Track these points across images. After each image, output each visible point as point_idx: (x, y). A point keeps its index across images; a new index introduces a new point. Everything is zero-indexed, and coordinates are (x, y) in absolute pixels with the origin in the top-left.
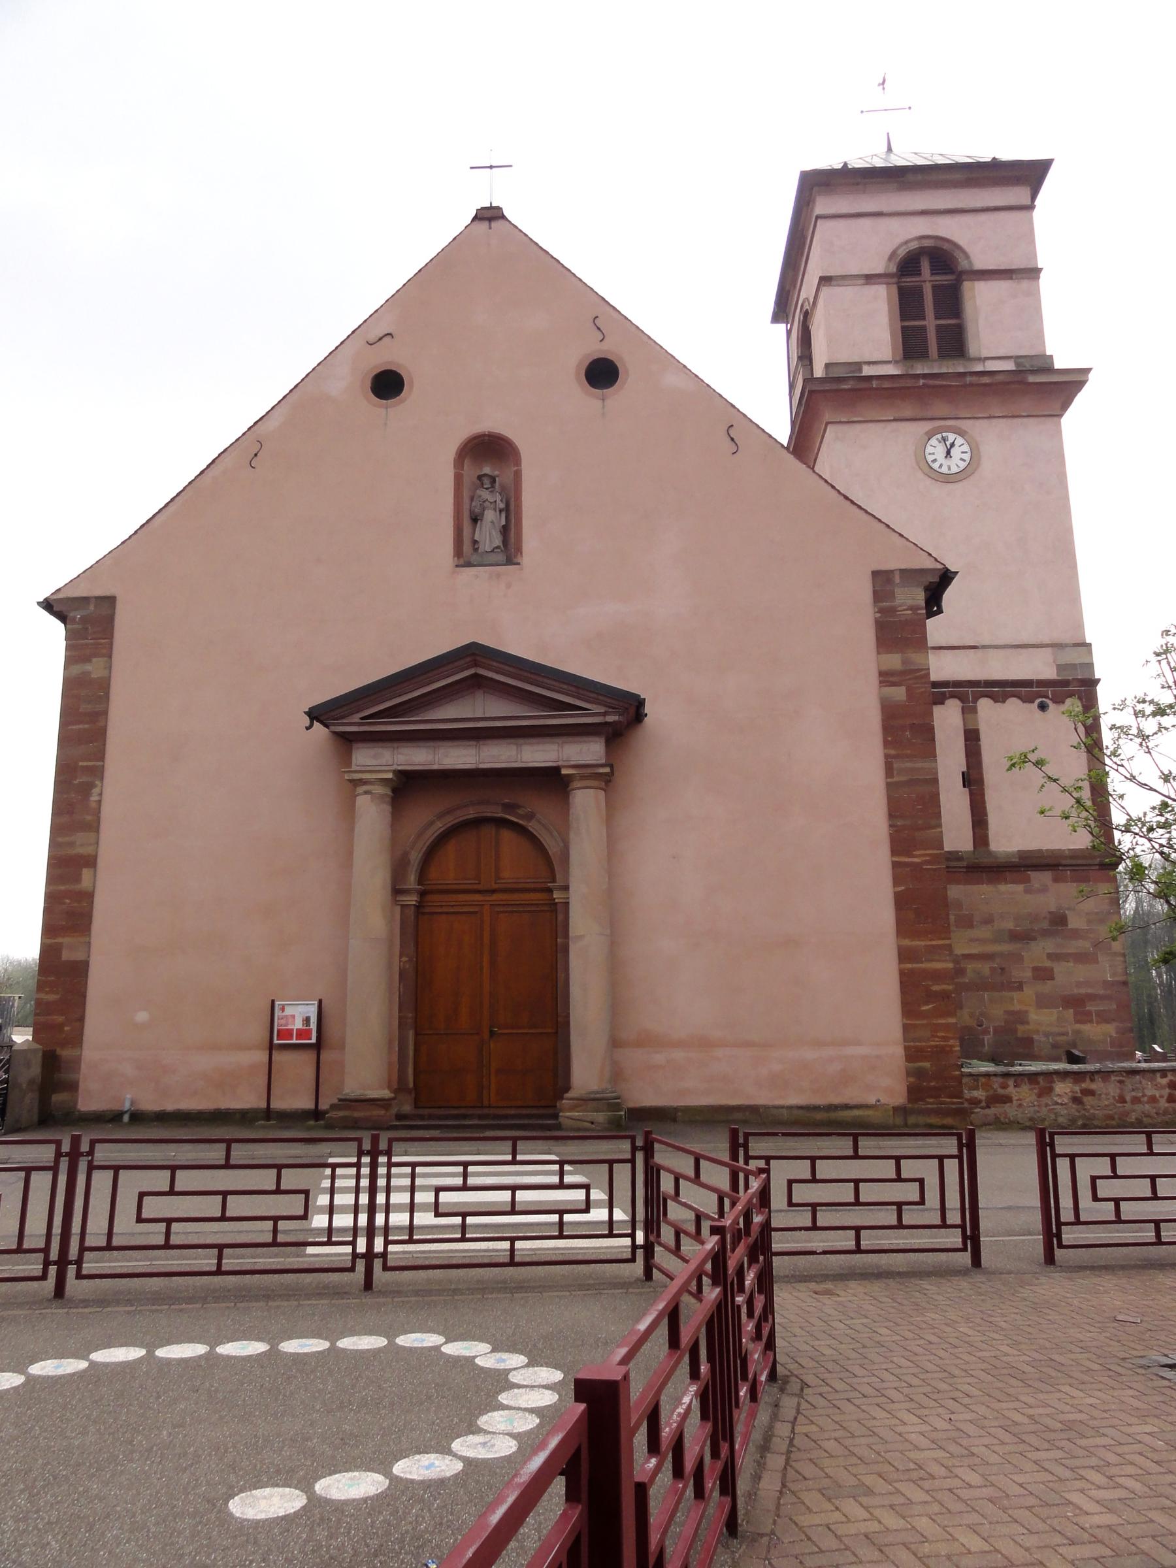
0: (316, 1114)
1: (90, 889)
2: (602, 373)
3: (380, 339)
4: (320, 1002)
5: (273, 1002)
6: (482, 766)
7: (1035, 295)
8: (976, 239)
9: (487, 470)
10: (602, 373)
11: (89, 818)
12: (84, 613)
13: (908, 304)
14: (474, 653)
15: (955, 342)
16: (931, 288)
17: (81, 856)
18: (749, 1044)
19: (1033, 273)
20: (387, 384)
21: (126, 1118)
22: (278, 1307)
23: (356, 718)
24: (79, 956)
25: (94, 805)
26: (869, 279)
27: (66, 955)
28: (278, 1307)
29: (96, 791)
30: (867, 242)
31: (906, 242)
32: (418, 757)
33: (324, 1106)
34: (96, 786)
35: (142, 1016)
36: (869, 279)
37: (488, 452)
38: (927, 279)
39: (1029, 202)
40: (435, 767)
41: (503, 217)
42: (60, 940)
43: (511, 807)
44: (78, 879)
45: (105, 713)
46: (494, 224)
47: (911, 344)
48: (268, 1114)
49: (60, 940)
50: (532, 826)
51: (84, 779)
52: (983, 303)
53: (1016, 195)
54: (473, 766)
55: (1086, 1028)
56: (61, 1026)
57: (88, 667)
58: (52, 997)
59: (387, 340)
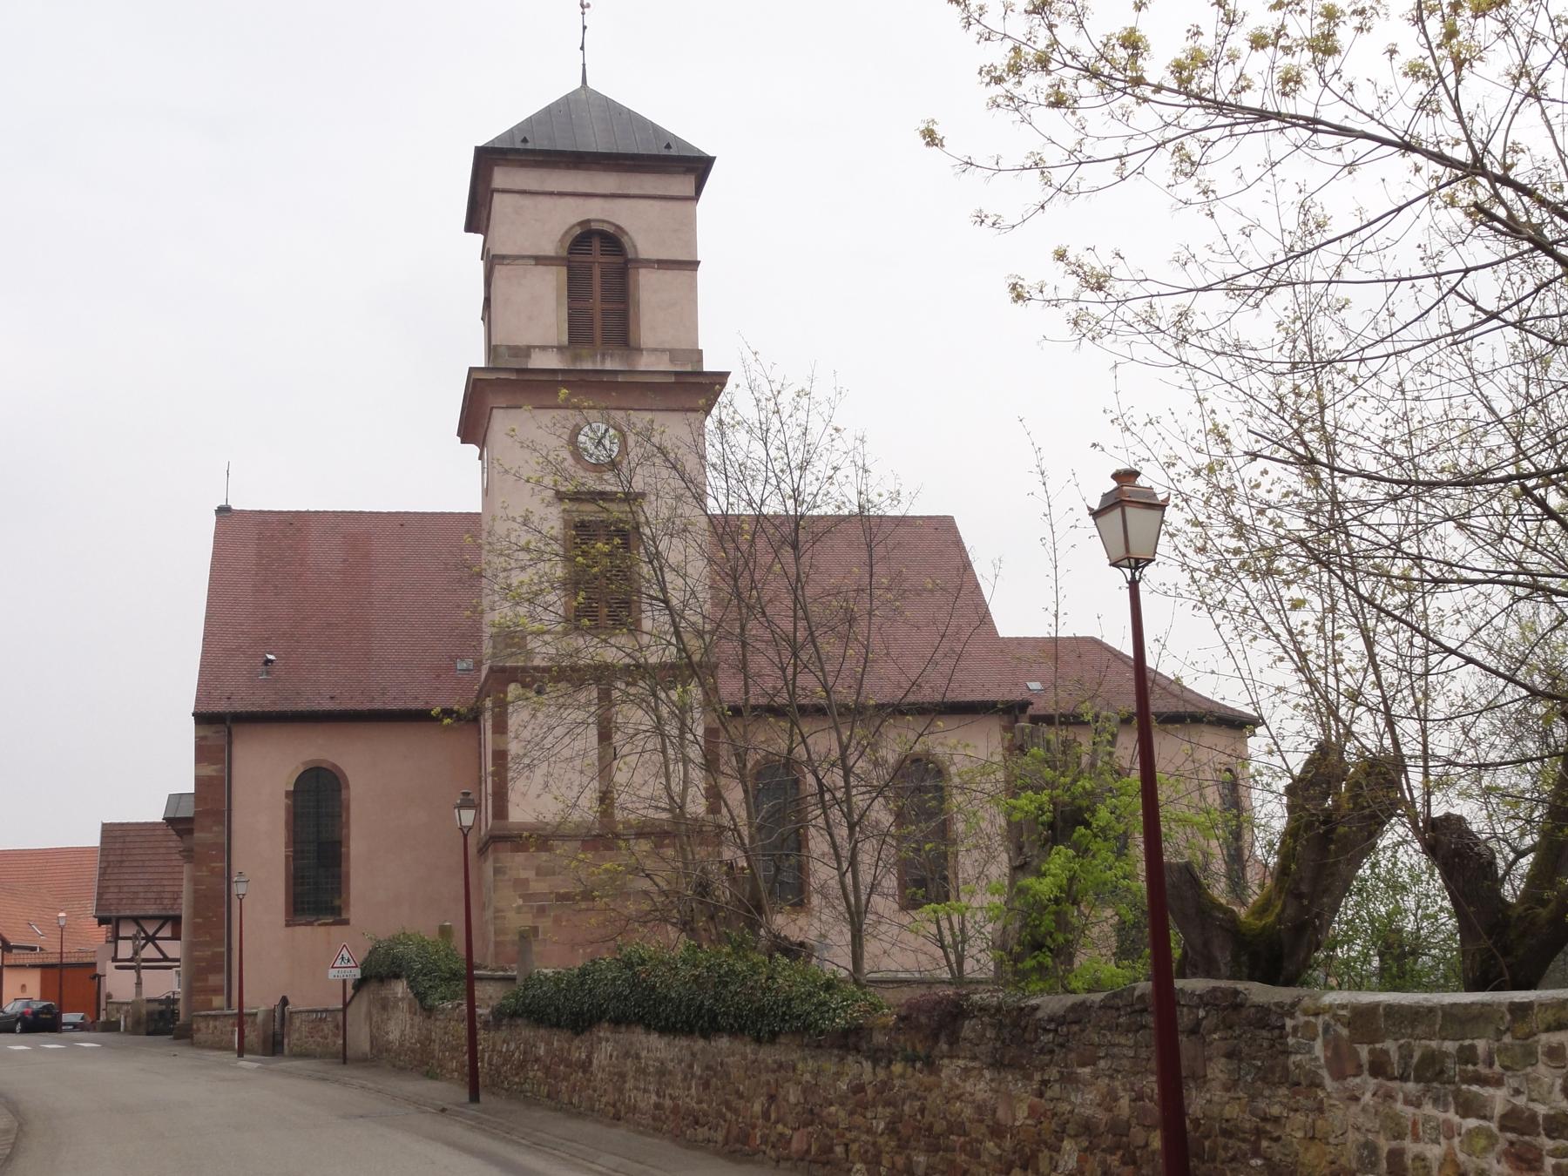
7: (693, 287)
8: (640, 221)
13: (576, 288)
15: (621, 333)
16: (602, 275)
18: (1433, 340)
19: (693, 265)
21: (18, 1027)
22: (1442, 471)
26: (540, 260)
28: (1442, 471)
30: (543, 217)
31: (566, 233)
36: (540, 260)
38: (597, 258)
39: (691, 192)
47: (579, 332)
52: (650, 288)
53: (684, 185)
55: (1033, 963)
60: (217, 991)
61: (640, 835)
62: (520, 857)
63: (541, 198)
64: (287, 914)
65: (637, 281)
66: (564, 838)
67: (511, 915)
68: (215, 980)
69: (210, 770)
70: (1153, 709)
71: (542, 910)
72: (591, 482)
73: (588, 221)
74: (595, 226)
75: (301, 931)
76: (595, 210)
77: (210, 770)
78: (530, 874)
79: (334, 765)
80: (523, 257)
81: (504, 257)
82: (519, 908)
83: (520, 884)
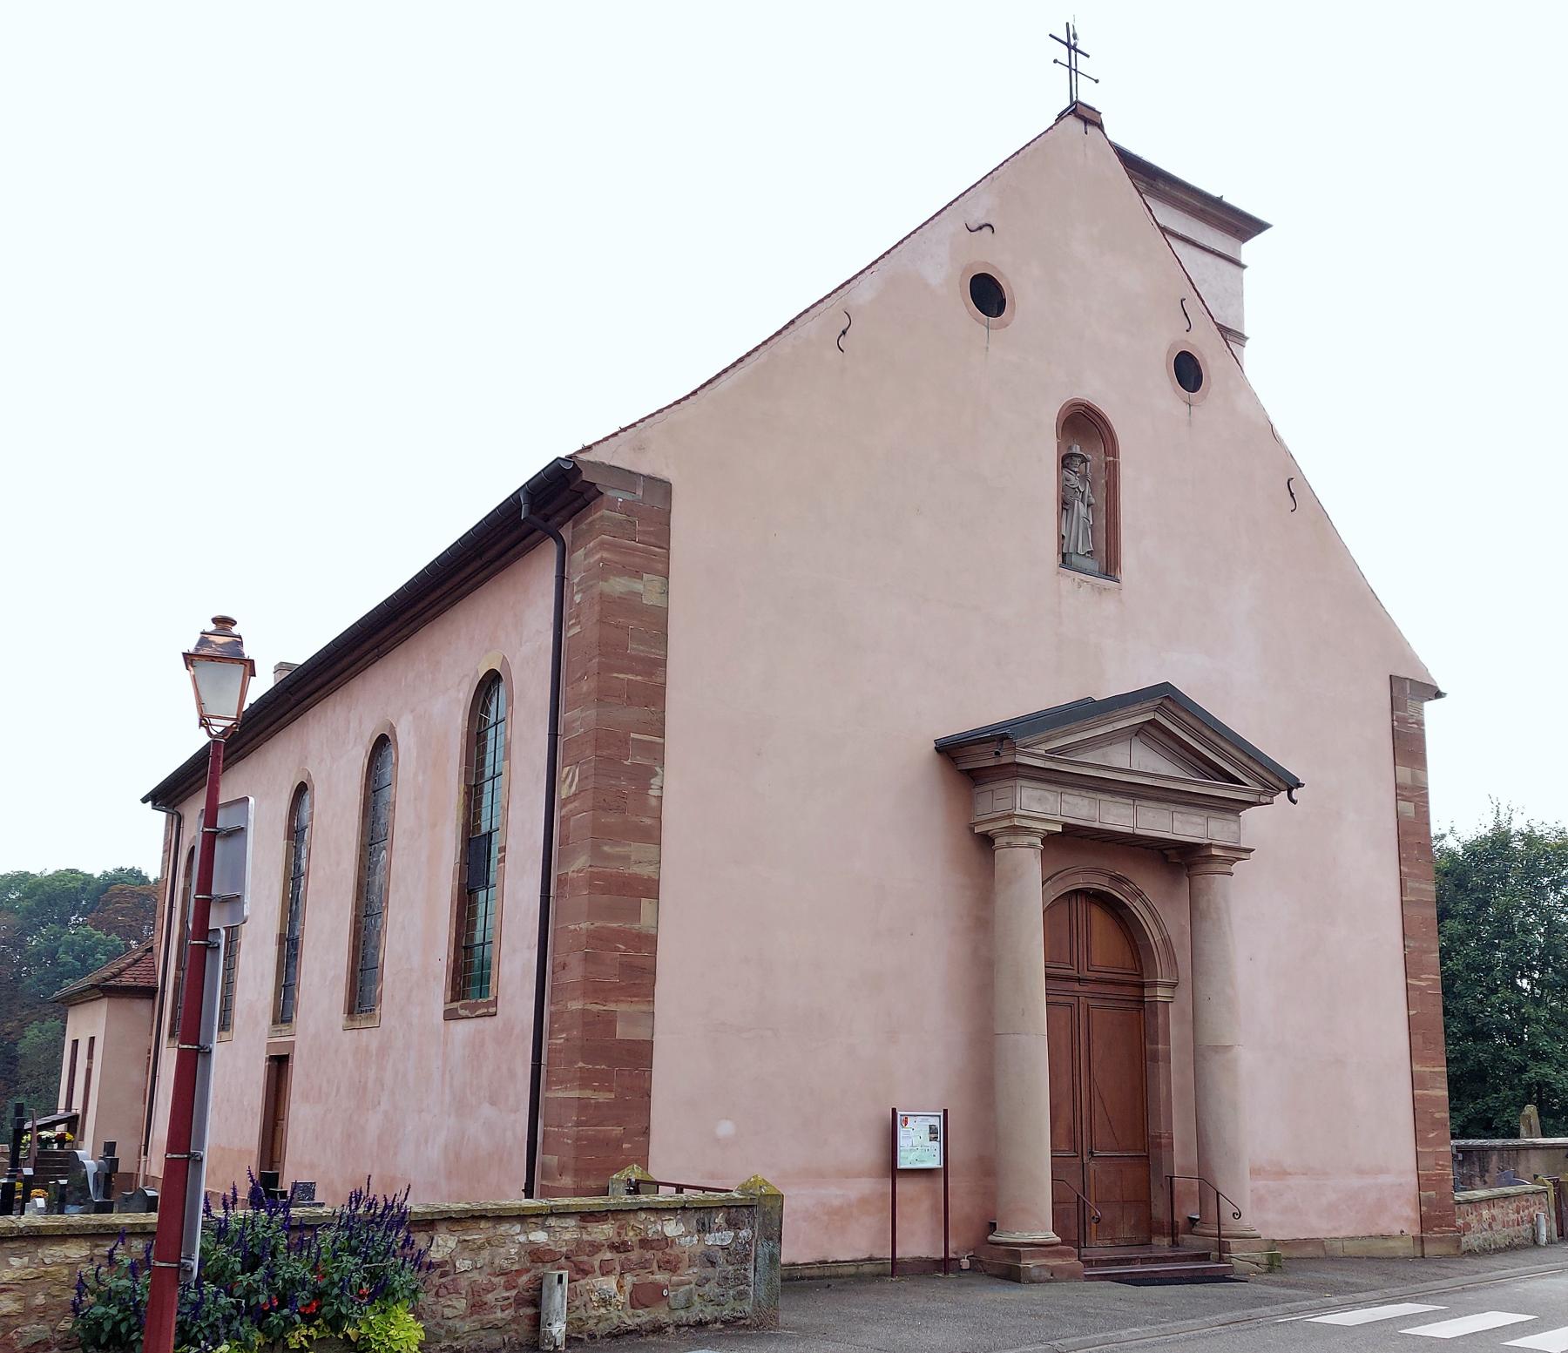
0: (945, 1266)
1: (653, 931)
2: (987, 295)
3: (980, 228)
4: (945, 1111)
5: (894, 1110)
6: (1138, 832)
9: (1077, 449)
10: (987, 295)
11: (648, 821)
12: (629, 497)
14: (1165, 696)
17: (637, 878)
20: (1188, 371)
23: (1041, 750)
24: (638, 1034)
25: (654, 802)
27: (622, 1031)
29: (655, 781)
32: (1081, 809)
33: (951, 1255)
34: (656, 774)
35: (726, 1128)
37: (1084, 426)
40: (1096, 825)
41: (1100, 126)
42: (612, 1007)
43: (1119, 880)
44: (636, 914)
45: (662, 663)
46: (1089, 128)
48: (897, 1269)
49: (612, 1007)
50: (1137, 907)
51: (639, 760)
54: (1130, 831)
56: (619, 1142)
57: (638, 586)
58: (603, 1097)
59: (987, 230)
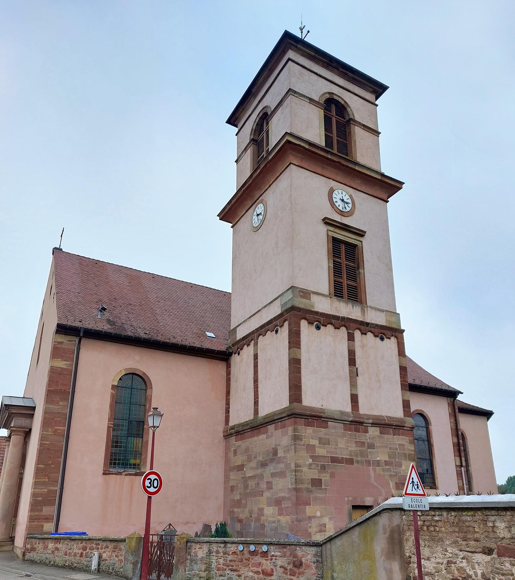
52: (359, 135)
60: (48, 519)
61: (374, 424)
62: (310, 430)
63: (312, 74)
64: (105, 464)
65: (354, 131)
66: (334, 419)
67: (305, 469)
68: (49, 510)
69: (61, 364)
70: (146, 485)
71: (323, 468)
72: (337, 218)
73: (333, 94)
74: (335, 97)
75: (113, 478)
76: (336, 90)
77: (61, 364)
78: (316, 442)
79: (144, 373)
80: (304, 96)
81: (295, 92)
82: (310, 465)
83: (310, 448)
